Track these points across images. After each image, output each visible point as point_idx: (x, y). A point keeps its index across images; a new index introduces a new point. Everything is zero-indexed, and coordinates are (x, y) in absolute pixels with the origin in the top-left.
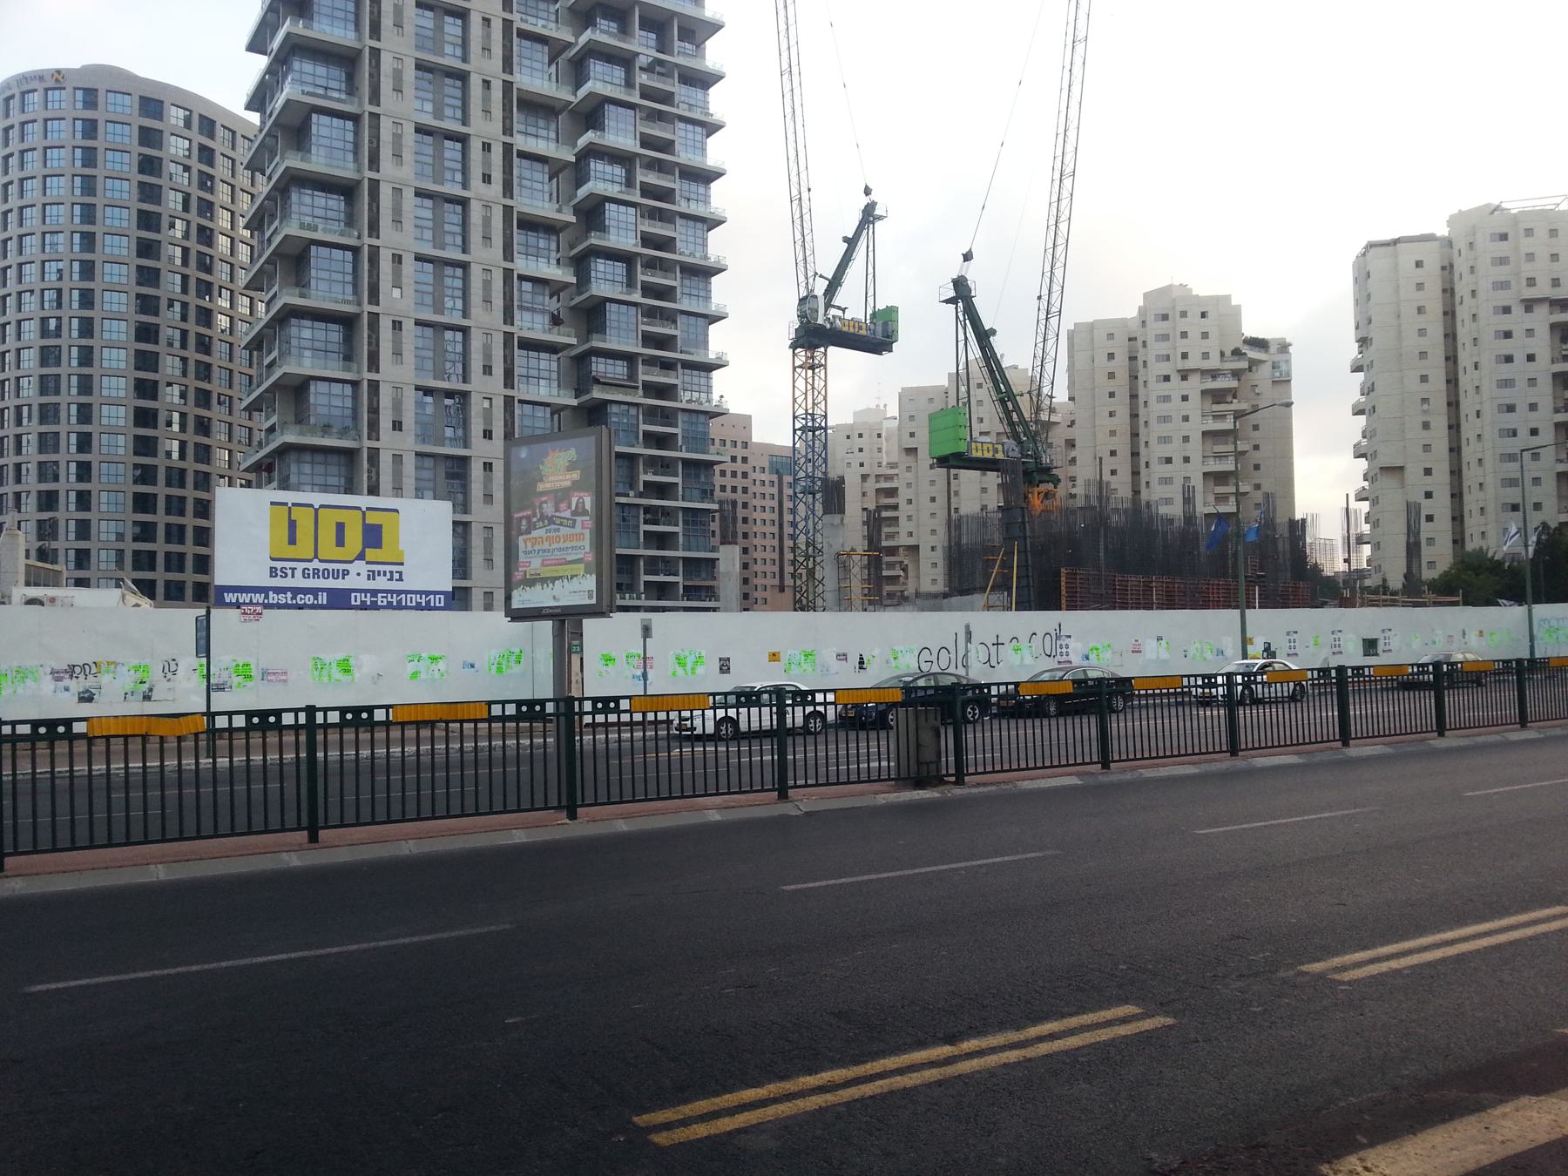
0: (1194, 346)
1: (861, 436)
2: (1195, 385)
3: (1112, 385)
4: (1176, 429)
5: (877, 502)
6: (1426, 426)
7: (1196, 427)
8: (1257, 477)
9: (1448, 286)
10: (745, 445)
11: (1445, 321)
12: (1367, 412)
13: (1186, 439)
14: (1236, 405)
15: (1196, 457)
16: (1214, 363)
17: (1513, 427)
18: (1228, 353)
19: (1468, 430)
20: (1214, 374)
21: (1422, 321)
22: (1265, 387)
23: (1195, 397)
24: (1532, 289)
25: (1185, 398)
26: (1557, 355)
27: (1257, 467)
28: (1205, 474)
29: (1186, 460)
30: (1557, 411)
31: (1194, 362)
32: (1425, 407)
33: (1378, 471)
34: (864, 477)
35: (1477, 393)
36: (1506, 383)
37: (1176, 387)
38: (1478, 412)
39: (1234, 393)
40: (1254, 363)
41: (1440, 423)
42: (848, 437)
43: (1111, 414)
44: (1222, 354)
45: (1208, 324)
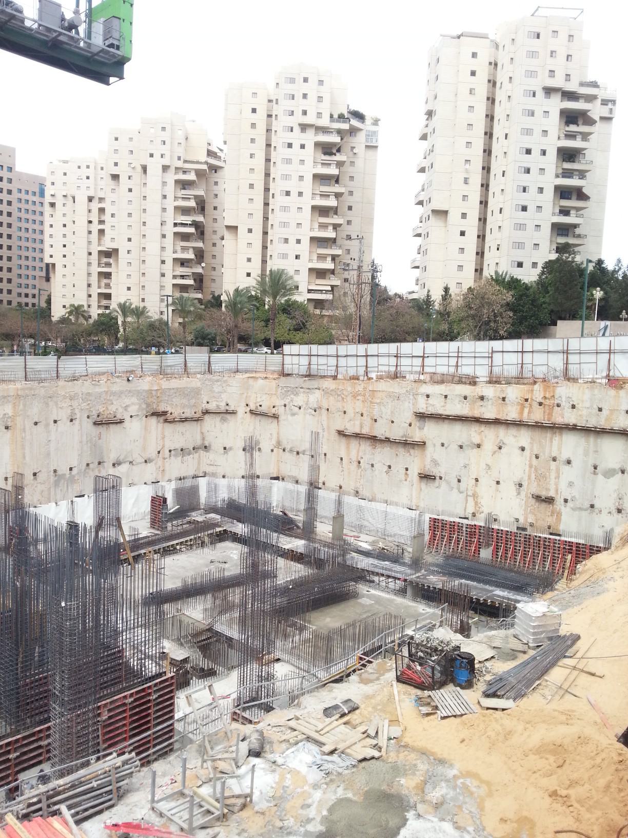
0: (311, 105)
1: (88, 167)
2: (310, 138)
3: (253, 133)
4: (292, 233)
5: (99, 218)
6: (466, 181)
7: (306, 234)
8: (350, 215)
9: (489, 113)
10: (10, 169)
11: (486, 121)
12: (423, 235)
13: (301, 178)
14: (339, 157)
15: (308, 193)
16: (325, 122)
17: (525, 185)
18: (336, 116)
19: (495, 185)
20: (324, 130)
21: (471, 100)
22: (360, 149)
23: (310, 147)
24: (552, 79)
25: (303, 146)
26: (560, 171)
27: (350, 208)
28: (310, 269)
29: (300, 194)
30: (557, 176)
31: (310, 119)
32: (467, 166)
33: (430, 213)
34: (90, 199)
35: (512, 63)
36: (521, 227)
37: (297, 137)
38: (501, 209)
39: (335, 211)
40: (353, 131)
41: (476, 179)
42: (79, 167)
43: (252, 156)
44: (331, 116)
45: (324, 91)
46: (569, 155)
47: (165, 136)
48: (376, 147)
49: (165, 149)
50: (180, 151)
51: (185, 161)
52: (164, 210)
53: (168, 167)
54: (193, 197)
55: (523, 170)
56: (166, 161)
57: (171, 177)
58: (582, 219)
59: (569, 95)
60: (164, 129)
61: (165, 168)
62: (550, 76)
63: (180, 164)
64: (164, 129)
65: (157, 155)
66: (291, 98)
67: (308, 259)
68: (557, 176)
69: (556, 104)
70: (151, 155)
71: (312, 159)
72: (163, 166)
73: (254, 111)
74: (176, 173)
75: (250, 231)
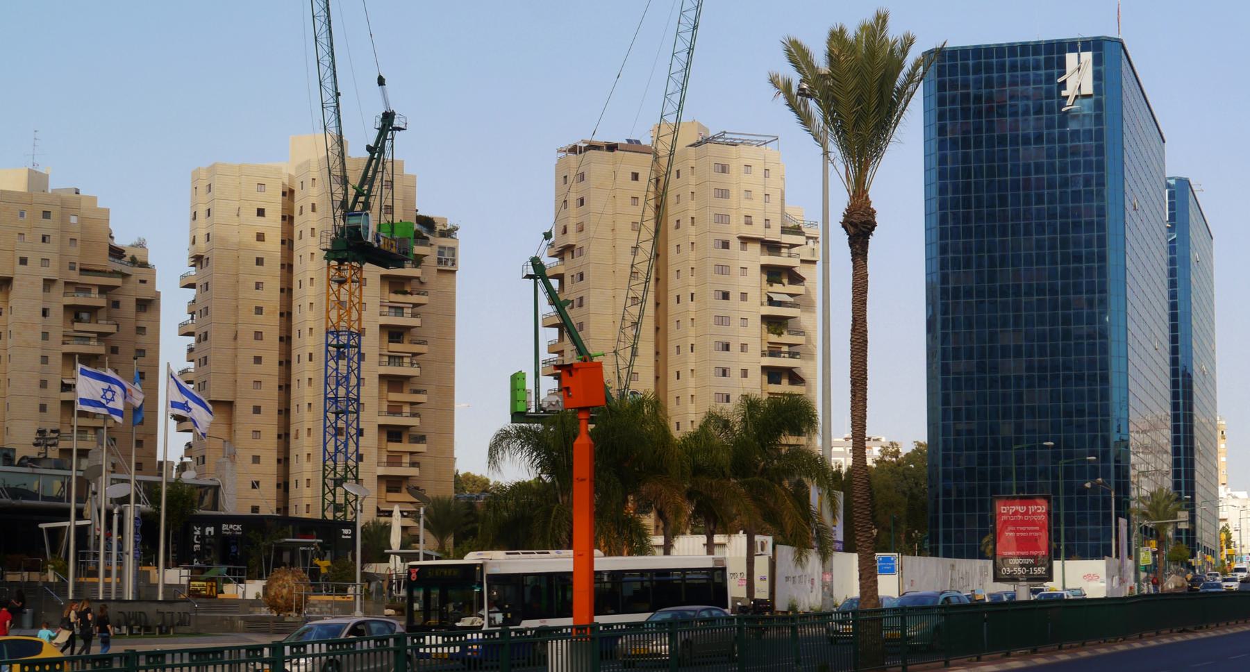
30: (763, 354)
46: (774, 324)
47: (48, 226)
48: (454, 272)
49: (50, 250)
50: (75, 254)
51: (84, 271)
52: (45, 359)
53: (53, 281)
54: (95, 335)
55: (720, 346)
56: (50, 273)
57: (59, 300)
58: (804, 337)
59: (772, 247)
60: (46, 214)
61: (48, 283)
62: (747, 223)
63: (75, 276)
64: (46, 214)
65: (34, 260)
66: (721, 374)
67: (375, 459)
68: (763, 354)
69: (756, 258)
70: (23, 261)
71: (378, 300)
72: (45, 280)
73: (261, 212)
74: (65, 294)
75: (257, 410)
